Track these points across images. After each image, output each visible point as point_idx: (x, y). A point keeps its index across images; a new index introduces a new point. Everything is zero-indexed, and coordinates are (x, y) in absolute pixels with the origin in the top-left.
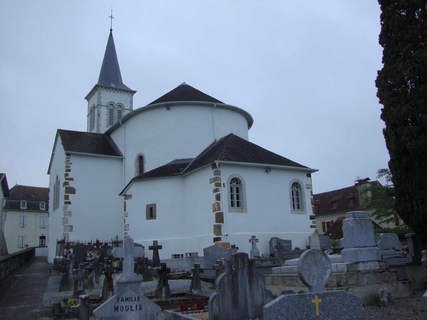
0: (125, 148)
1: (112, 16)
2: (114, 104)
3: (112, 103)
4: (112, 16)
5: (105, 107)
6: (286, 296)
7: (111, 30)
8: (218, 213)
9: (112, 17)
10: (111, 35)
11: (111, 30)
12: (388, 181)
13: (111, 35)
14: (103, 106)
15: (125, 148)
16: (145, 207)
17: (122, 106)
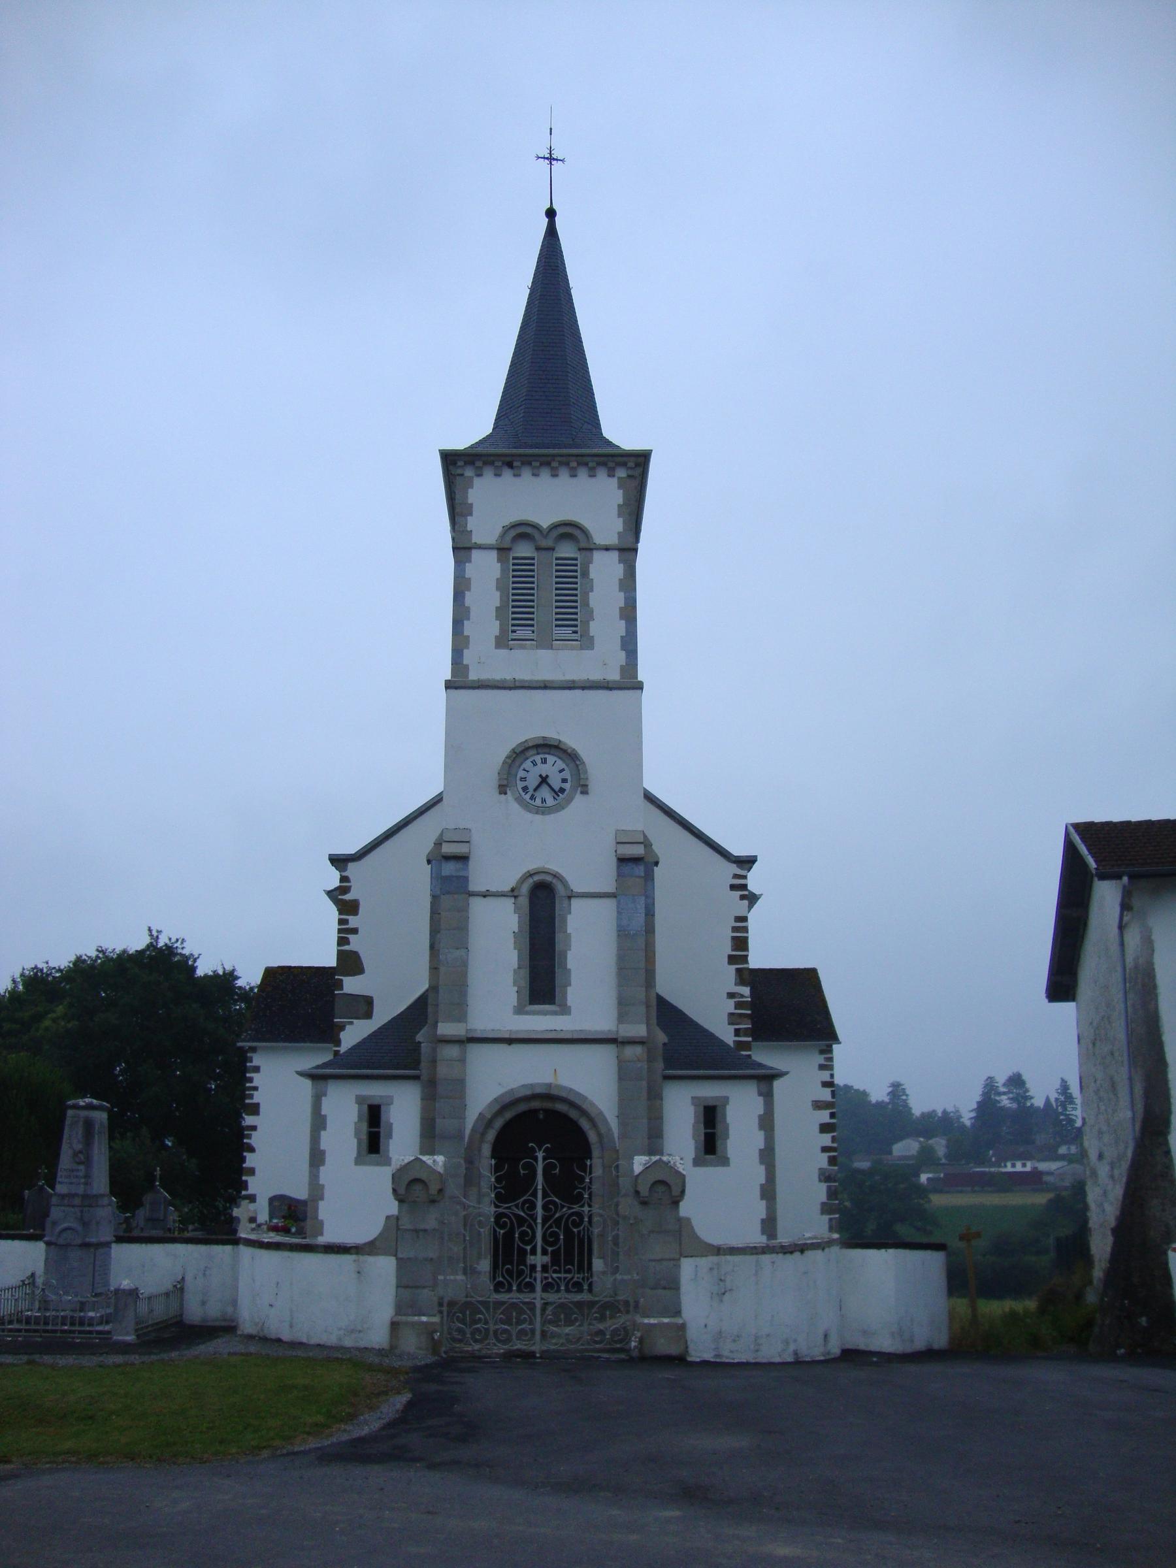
0: (570, 686)
1: (550, 154)
2: (537, 535)
3: (529, 530)
4: (550, 154)
5: (490, 551)
6: (559, 1326)
7: (551, 213)
8: (738, 1001)
9: (551, 159)
10: (551, 233)
11: (551, 213)
12: (831, 1229)
13: (551, 233)
14: (480, 547)
15: (570, 686)
16: (261, 1113)
17: (576, 532)
